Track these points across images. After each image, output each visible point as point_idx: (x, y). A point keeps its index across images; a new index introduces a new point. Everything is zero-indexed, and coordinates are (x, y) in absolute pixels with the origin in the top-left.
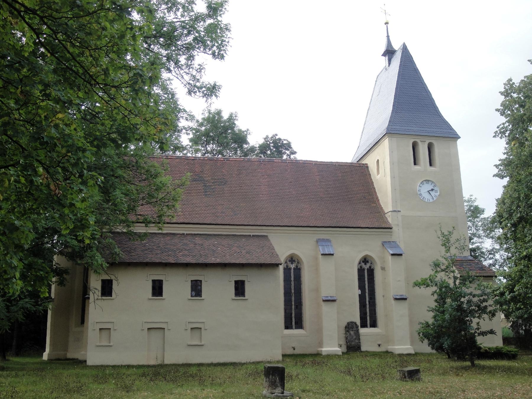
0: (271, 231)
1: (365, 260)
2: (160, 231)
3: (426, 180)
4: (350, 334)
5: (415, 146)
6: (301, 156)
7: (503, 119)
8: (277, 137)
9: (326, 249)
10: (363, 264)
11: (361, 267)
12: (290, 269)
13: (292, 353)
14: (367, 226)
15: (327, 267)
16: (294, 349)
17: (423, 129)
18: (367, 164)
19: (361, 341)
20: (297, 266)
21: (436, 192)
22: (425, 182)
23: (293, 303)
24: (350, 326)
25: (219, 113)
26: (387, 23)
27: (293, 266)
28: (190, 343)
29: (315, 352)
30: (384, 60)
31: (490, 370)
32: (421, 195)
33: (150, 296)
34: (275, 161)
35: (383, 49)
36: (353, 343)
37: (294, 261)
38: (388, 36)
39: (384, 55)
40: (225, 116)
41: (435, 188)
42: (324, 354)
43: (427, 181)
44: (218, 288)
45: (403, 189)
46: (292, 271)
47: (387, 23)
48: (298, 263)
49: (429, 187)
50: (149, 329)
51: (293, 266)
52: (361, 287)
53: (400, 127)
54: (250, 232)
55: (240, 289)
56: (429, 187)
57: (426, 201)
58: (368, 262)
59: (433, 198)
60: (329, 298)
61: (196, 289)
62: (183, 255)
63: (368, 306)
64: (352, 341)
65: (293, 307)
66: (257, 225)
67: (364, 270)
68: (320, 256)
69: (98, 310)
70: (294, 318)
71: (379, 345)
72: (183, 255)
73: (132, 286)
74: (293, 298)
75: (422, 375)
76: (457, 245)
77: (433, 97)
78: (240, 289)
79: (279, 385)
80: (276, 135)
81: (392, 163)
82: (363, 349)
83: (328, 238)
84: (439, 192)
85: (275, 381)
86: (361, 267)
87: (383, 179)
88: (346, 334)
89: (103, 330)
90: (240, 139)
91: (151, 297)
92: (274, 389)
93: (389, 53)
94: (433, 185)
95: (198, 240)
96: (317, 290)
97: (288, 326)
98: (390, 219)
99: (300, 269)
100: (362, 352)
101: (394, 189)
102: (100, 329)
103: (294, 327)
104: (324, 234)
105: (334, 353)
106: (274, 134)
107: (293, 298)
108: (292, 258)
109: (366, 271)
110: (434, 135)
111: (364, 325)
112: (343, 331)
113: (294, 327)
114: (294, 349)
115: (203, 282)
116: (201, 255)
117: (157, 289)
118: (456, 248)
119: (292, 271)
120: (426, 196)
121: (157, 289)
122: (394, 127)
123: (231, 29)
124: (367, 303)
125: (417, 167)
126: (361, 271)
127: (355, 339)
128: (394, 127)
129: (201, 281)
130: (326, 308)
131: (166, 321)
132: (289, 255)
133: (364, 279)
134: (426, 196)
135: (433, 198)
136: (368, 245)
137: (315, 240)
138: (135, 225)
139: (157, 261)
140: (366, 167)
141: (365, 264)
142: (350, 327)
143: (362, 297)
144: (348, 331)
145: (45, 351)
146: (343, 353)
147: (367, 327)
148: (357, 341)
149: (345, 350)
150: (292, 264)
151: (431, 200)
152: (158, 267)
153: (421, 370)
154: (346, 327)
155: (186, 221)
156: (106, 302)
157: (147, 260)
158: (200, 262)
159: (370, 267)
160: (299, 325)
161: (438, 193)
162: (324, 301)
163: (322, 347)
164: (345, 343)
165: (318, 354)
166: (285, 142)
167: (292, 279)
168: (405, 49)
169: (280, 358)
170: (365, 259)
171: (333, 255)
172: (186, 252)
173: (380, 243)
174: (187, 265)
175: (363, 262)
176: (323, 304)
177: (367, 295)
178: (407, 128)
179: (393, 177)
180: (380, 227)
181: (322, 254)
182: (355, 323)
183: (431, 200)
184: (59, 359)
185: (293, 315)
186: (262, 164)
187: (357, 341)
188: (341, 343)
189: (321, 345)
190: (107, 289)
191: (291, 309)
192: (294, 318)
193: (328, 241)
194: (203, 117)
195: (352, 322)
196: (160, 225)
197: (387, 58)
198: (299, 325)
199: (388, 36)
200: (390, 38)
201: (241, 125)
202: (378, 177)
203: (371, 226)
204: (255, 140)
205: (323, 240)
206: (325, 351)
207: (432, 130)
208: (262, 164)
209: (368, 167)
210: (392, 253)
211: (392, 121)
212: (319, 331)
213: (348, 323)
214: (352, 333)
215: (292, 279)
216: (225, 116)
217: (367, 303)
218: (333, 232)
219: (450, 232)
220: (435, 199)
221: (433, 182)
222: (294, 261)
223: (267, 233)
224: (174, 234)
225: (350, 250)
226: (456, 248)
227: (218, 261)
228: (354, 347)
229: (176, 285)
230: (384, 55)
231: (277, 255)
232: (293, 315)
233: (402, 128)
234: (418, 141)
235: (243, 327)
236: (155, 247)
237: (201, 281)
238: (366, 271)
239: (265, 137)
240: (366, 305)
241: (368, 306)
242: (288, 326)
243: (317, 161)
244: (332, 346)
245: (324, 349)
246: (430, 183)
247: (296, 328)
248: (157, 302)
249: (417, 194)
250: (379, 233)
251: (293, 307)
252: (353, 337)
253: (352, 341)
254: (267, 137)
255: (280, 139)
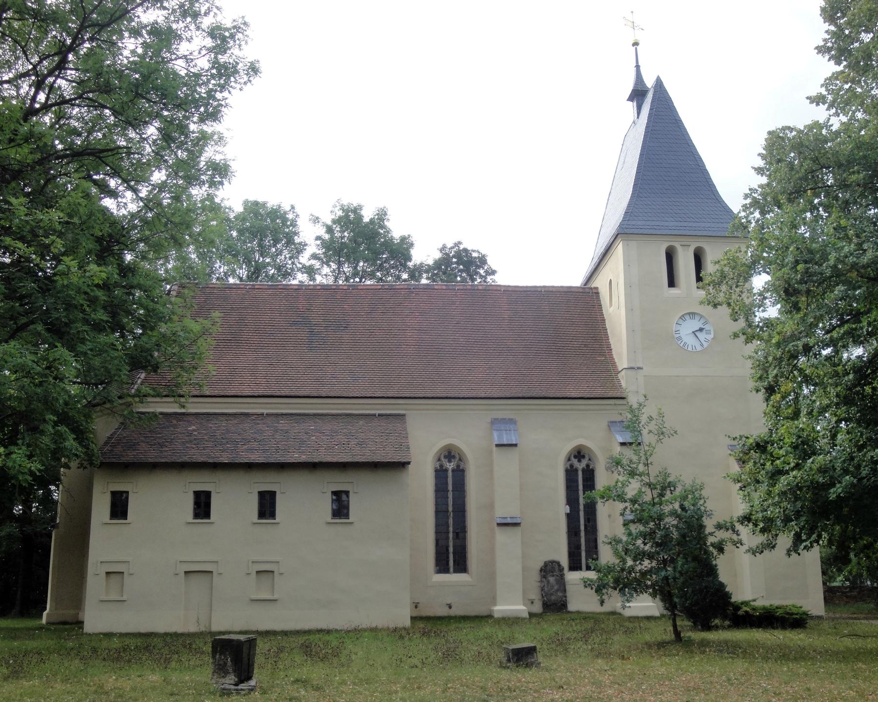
0: (412, 407)
1: (579, 454)
2: (183, 411)
3: (689, 314)
4: (548, 582)
5: (670, 257)
6: (503, 279)
7: (232, 197)
8: (462, 247)
9: (505, 436)
10: (575, 462)
11: (572, 466)
12: (447, 470)
13: (446, 614)
14: (580, 396)
15: (506, 466)
16: (450, 607)
17: (686, 224)
18: (597, 288)
19: (568, 594)
20: (458, 466)
21: (708, 332)
22: (687, 317)
23: (451, 529)
24: (548, 568)
25: (356, 211)
26: (636, 44)
27: (450, 466)
28: (254, 597)
29: (485, 614)
30: (631, 106)
31: (732, 649)
32: (680, 338)
33: (329, 518)
34: (436, 287)
35: (629, 87)
36: (553, 598)
37: (454, 457)
38: (638, 67)
39: (631, 99)
40: (367, 215)
41: (707, 327)
42: (496, 615)
43: (692, 315)
44: (304, 502)
45: (650, 332)
46: (450, 474)
47: (636, 44)
48: (460, 460)
49: (696, 324)
50: (258, 572)
51: (450, 466)
52: (572, 500)
53: (644, 223)
54: (262, 408)
55: (341, 507)
56: (696, 324)
57: (690, 349)
58: (584, 457)
59: (702, 345)
60: (509, 521)
61: (267, 506)
62: (247, 450)
63: (583, 534)
64: (552, 594)
65: (451, 535)
66: (388, 398)
67: (577, 470)
68: (495, 448)
69: (105, 542)
70: (451, 553)
71: (532, 603)
72: (247, 450)
73: (159, 503)
74: (451, 521)
75: (540, 657)
76: (652, 426)
77: (708, 167)
78: (341, 507)
79: (231, 670)
80: (460, 243)
81: (628, 285)
82: (572, 607)
83: (511, 417)
84: (712, 333)
85: (225, 664)
86: (572, 466)
87: (616, 312)
88: (541, 581)
89: (112, 576)
90: (400, 251)
91: (191, 520)
92: (223, 677)
93: (638, 94)
94: (702, 321)
95: (283, 424)
96: (490, 506)
97: (442, 566)
98: (624, 380)
99: (463, 471)
100: (569, 612)
101: (631, 330)
102: (108, 573)
103: (452, 570)
104: (504, 410)
105: (515, 615)
106: (456, 241)
107: (451, 521)
108: (450, 453)
109: (580, 474)
110: (705, 233)
111: (575, 566)
112: (535, 576)
113: (452, 570)
114: (450, 607)
115: (351, 494)
116: (277, 450)
117: (202, 506)
118: (650, 431)
119: (450, 474)
120: (690, 341)
121: (202, 506)
122: (634, 223)
123: (262, 69)
124: (582, 528)
125: (673, 291)
126: (571, 473)
127: (557, 590)
128: (634, 223)
129: (127, 492)
130: (502, 537)
131: (126, 559)
132: (445, 446)
133: (577, 486)
134: (690, 341)
135: (702, 345)
136: (592, 430)
137: (489, 420)
138: (149, 399)
139: (201, 459)
140: (596, 293)
141: (579, 461)
142: (550, 569)
143: (572, 519)
144: (544, 577)
145: (45, 609)
146: (531, 615)
147: (581, 569)
148: (560, 594)
149: (538, 608)
150: (450, 461)
151: (699, 348)
152: (202, 469)
153: (538, 647)
154: (541, 570)
155: (270, 393)
156: (118, 528)
157: (186, 459)
158: (272, 460)
159: (588, 466)
160: (461, 566)
161: (712, 336)
162: (499, 524)
163: (495, 605)
164: (540, 597)
165: (486, 618)
166: (475, 255)
167: (450, 488)
168: (659, 84)
169: (408, 623)
170: (579, 452)
171: (516, 445)
172: (255, 445)
173: (604, 424)
174: (250, 467)
175: (575, 457)
176: (497, 529)
177: (582, 514)
178: (658, 223)
179: (630, 310)
180: (605, 396)
181: (497, 445)
182: (558, 563)
183: (699, 348)
184: (65, 623)
185: (451, 549)
186: (412, 292)
187: (560, 594)
188: (533, 597)
189: (494, 602)
190: (119, 508)
191: (448, 538)
192: (451, 553)
193: (512, 421)
194: (333, 217)
195: (553, 562)
196: (182, 400)
197: (635, 103)
198: (461, 566)
199: (638, 67)
200: (641, 68)
201: (396, 229)
202: (611, 310)
203: (588, 396)
204: (424, 253)
205: (504, 421)
206: (499, 611)
207: (703, 225)
208: (412, 292)
209: (598, 293)
210: (622, 441)
211: (629, 214)
212: (492, 576)
213: (545, 563)
214: (552, 579)
215: (450, 488)
216: (367, 215)
217: (582, 528)
218: (519, 407)
219: (641, 405)
220: (705, 345)
221: (701, 317)
222: (454, 457)
223: (406, 410)
224: (247, 415)
225: (549, 438)
226: (650, 431)
227: (304, 458)
228: (555, 604)
229: (234, 499)
230: (631, 99)
231: (408, 447)
232: (451, 549)
233: (648, 223)
234: (677, 245)
235: (346, 568)
236: (206, 437)
237: (127, 492)
238: (580, 474)
239: (440, 246)
240: (580, 531)
241: (583, 534)
242: (442, 566)
243: (509, 286)
244: (512, 604)
245: (497, 608)
246: (697, 318)
247: (455, 571)
248: (202, 528)
249: (674, 337)
250: (603, 407)
251: (451, 535)
252: (553, 586)
253: (552, 594)
254: (444, 247)
255: (466, 250)
